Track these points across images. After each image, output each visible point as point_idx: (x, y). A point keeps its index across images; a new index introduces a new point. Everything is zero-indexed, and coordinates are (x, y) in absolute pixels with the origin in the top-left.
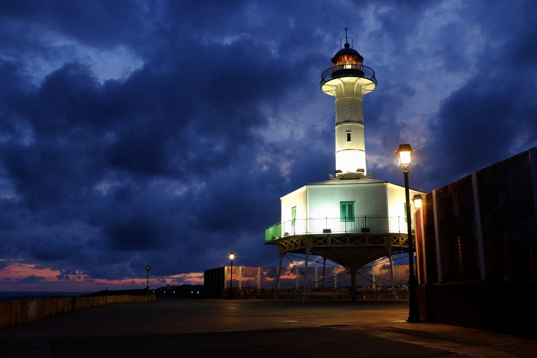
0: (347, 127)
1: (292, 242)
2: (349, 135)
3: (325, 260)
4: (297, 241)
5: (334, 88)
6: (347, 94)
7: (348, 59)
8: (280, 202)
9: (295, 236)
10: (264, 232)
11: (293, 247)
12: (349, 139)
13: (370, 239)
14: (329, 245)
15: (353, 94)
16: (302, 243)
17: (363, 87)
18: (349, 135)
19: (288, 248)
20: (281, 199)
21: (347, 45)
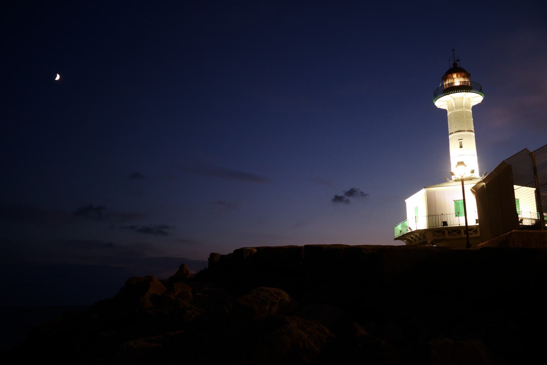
0: (459, 136)
1: (416, 236)
2: (461, 143)
3: (468, 245)
4: (420, 235)
5: (446, 103)
6: (457, 107)
7: (457, 76)
8: (405, 203)
9: (417, 231)
10: (394, 230)
11: (418, 240)
12: (461, 147)
13: (449, 232)
14: (447, 236)
15: (453, 108)
16: (424, 235)
17: (471, 100)
18: (461, 143)
19: (413, 242)
20: (406, 201)
21: (455, 64)
